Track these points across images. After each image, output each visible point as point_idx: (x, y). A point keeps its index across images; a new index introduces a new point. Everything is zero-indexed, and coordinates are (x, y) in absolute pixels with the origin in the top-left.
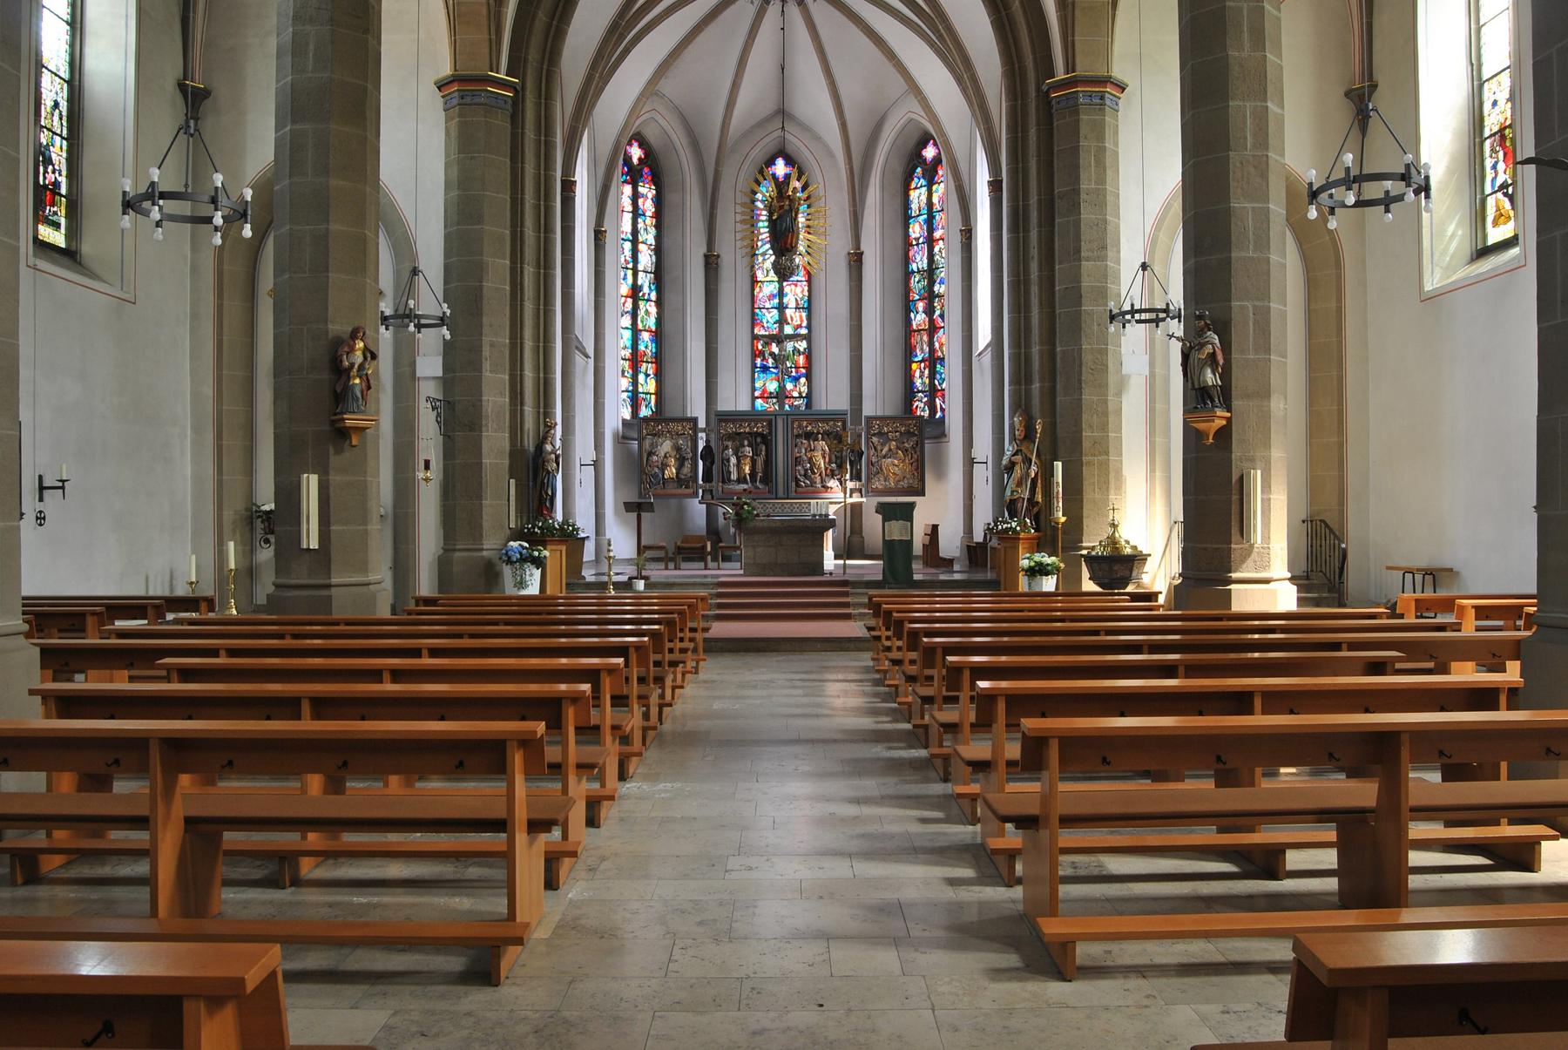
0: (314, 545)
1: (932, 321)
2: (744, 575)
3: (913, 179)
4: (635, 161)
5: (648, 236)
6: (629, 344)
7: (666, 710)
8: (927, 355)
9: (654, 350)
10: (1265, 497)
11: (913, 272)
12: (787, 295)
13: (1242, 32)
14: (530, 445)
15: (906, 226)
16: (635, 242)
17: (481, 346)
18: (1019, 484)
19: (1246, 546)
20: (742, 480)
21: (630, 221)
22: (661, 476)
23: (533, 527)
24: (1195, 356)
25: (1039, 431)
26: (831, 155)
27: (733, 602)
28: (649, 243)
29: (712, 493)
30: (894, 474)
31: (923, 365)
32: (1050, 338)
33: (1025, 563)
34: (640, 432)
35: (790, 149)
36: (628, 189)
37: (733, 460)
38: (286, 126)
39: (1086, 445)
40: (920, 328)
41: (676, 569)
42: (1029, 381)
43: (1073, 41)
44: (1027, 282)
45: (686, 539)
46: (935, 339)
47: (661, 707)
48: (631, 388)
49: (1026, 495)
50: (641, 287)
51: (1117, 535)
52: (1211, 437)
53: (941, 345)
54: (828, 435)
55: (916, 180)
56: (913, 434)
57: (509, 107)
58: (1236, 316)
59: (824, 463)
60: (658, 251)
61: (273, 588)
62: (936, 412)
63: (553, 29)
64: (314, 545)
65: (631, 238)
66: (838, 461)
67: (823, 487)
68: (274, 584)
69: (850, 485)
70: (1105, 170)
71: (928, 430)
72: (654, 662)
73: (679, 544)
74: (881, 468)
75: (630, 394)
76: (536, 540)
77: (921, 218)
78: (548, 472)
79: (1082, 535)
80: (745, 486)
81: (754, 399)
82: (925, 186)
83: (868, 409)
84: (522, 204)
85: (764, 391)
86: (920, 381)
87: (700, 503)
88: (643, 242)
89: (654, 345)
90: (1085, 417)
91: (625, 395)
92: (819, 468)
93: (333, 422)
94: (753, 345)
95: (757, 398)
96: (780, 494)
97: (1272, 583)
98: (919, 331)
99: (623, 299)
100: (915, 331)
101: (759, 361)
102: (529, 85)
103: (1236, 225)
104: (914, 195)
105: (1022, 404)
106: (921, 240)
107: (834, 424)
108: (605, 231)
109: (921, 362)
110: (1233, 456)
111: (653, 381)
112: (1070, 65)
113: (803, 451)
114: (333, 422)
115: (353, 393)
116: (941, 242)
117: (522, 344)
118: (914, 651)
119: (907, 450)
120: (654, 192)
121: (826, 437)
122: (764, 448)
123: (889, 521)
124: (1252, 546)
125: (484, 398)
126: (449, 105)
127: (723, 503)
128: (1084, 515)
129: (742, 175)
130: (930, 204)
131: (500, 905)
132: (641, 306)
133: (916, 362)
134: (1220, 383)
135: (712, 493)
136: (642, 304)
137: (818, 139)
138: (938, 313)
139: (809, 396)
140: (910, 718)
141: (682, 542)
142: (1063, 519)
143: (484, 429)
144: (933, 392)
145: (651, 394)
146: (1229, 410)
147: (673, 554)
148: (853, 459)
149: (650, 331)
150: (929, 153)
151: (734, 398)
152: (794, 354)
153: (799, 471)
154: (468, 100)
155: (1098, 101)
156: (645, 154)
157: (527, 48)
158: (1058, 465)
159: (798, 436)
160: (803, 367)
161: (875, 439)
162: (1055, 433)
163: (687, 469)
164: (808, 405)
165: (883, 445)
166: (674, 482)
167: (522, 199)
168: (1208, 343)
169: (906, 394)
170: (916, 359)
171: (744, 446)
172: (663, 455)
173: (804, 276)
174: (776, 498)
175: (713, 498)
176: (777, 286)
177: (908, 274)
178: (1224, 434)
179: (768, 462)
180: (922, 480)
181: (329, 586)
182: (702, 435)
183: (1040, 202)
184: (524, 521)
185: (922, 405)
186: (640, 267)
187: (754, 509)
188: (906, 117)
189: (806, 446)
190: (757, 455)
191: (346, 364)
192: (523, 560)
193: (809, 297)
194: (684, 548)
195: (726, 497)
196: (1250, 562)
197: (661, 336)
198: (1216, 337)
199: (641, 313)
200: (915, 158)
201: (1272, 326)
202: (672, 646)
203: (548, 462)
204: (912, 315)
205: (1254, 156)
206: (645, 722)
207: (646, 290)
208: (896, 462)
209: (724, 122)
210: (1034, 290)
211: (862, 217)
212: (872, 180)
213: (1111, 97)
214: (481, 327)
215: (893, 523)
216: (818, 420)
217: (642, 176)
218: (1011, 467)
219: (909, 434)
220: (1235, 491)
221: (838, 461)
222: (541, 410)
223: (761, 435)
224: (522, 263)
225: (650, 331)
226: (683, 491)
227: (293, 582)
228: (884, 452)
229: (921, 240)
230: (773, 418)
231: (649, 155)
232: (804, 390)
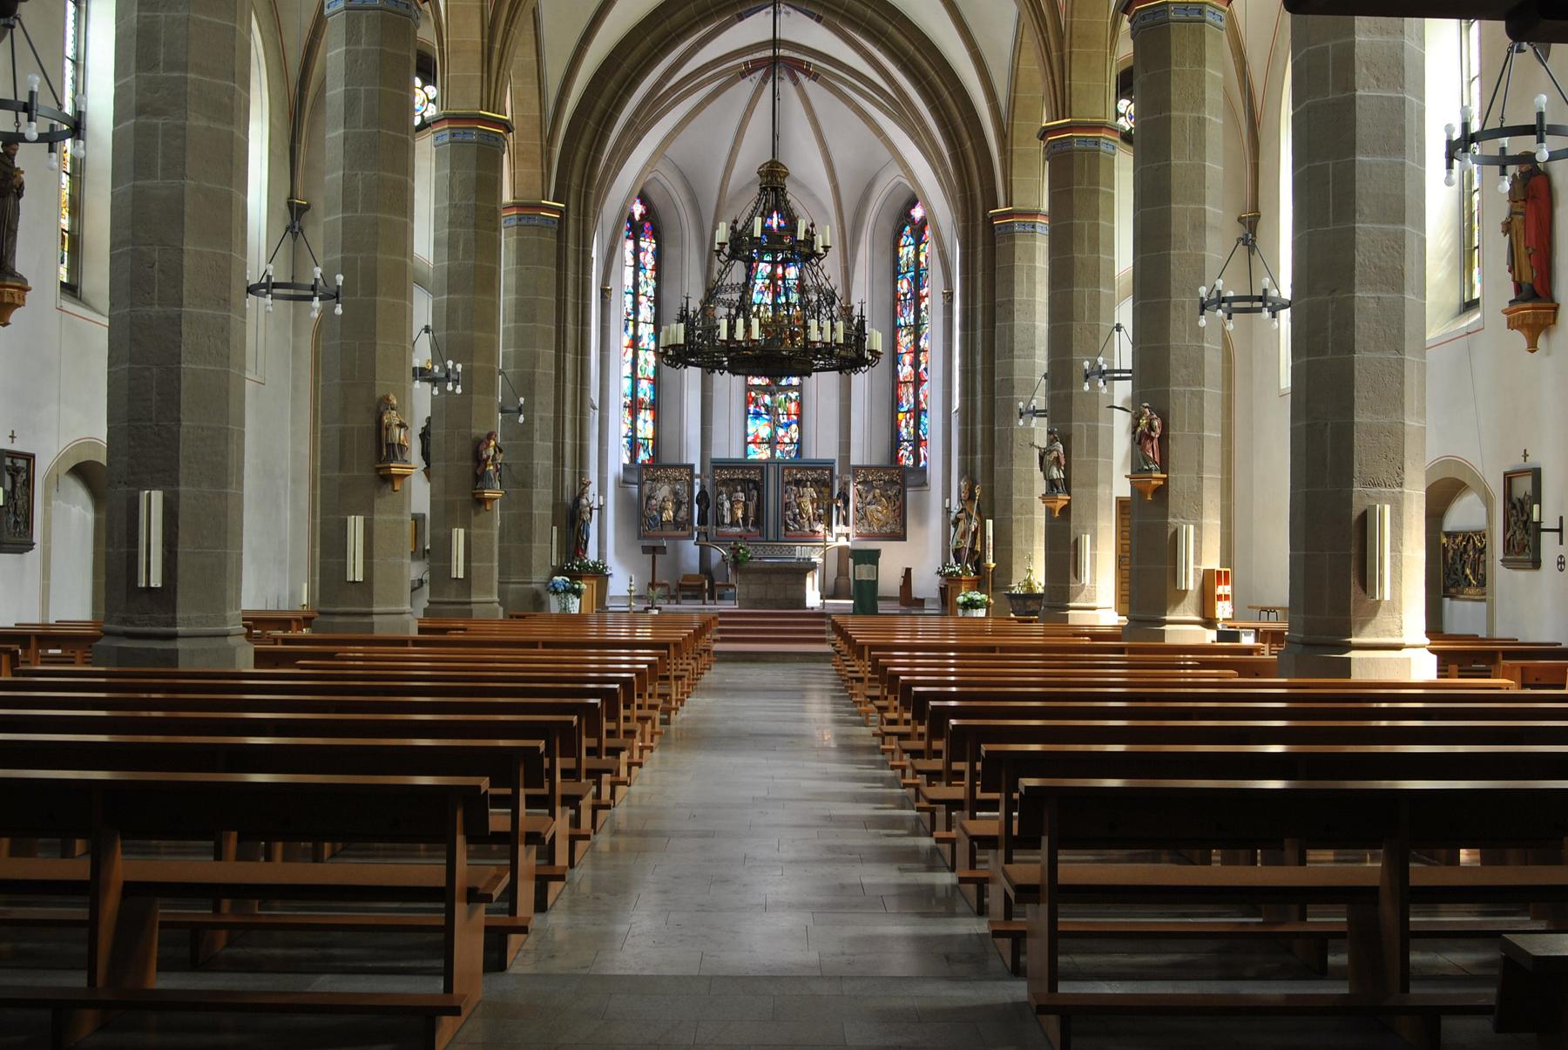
0: (461, 576)
2: (739, 608)
4: (637, 217)
5: (648, 288)
6: (628, 391)
7: (602, 814)
8: (912, 406)
9: (652, 397)
10: (1093, 552)
11: (901, 326)
13: (1083, 240)
14: (568, 498)
16: (636, 294)
17: (533, 420)
18: (963, 536)
19: (1080, 585)
20: (734, 523)
21: (632, 275)
22: (659, 518)
23: (572, 565)
24: (1047, 458)
25: (978, 494)
26: (825, 212)
27: (731, 627)
28: (649, 294)
29: (706, 536)
30: (878, 519)
31: (908, 415)
32: (990, 419)
33: (960, 599)
34: (640, 476)
36: (630, 245)
37: (727, 505)
38: (442, 295)
39: (1016, 506)
40: (906, 380)
41: (677, 603)
42: (974, 452)
43: (1011, 180)
44: (974, 372)
45: (686, 577)
47: (573, 840)
48: (630, 434)
49: (968, 545)
50: (641, 337)
51: (1032, 578)
52: (1057, 512)
53: (926, 397)
54: (816, 483)
55: (905, 238)
57: (556, 226)
58: (1075, 432)
61: (428, 604)
62: (919, 461)
63: (590, 158)
64: (461, 576)
65: (632, 291)
67: (811, 531)
68: (428, 601)
70: (1035, 285)
71: (911, 479)
72: (608, 732)
73: (680, 581)
74: (865, 514)
75: (629, 439)
76: (575, 576)
77: (909, 275)
78: (584, 521)
79: (1012, 578)
80: (738, 530)
81: (746, 444)
83: (856, 459)
84: (565, 304)
85: (757, 437)
86: (905, 430)
87: (695, 544)
88: (643, 295)
89: (652, 393)
90: (1015, 484)
91: (625, 441)
92: (807, 513)
93: (474, 494)
94: (746, 394)
95: (750, 443)
96: (771, 537)
97: (1403, 650)
98: (905, 382)
100: (901, 383)
101: (752, 408)
102: (571, 206)
103: (1076, 371)
104: (903, 252)
105: (967, 472)
107: (822, 473)
108: (611, 290)
109: (907, 412)
110: (1072, 525)
112: (1009, 203)
113: (793, 497)
114: (474, 494)
115: (490, 475)
116: (926, 299)
117: (563, 417)
118: (997, 792)
119: (890, 498)
120: (654, 246)
124: (1084, 585)
125: (535, 462)
126: (439, 142)
127: (717, 545)
128: (1014, 562)
131: (439, 984)
132: (640, 357)
134: (1062, 476)
135: (706, 536)
136: (641, 353)
137: (812, 195)
138: (923, 366)
139: (800, 442)
140: (933, 828)
141: (683, 580)
142: (993, 565)
143: (534, 486)
144: (917, 442)
145: (648, 439)
146: (1069, 495)
147: (676, 590)
150: (917, 213)
151: (727, 447)
152: (786, 402)
154: (524, 222)
155: (1031, 229)
157: (570, 177)
158: (990, 523)
159: (789, 483)
161: (859, 487)
162: (993, 494)
163: (683, 513)
164: (799, 452)
167: (566, 300)
168: (1054, 450)
169: (892, 442)
170: (902, 410)
172: (661, 499)
174: (767, 541)
175: (707, 540)
178: (1066, 510)
179: (760, 508)
180: (904, 526)
181: (470, 603)
182: (697, 481)
183: (984, 307)
184: (564, 559)
185: (907, 454)
186: (641, 318)
187: (748, 552)
188: (895, 180)
191: (485, 456)
192: (567, 591)
194: (686, 586)
195: (721, 540)
196: (1082, 595)
198: (1061, 446)
199: (641, 362)
200: (904, 217)
201: (1099, 438)
202: (629, 714)
203: (584, 513)
204: (899, 367)
205: (1089, 325)
206: (595, 800)
209: (722, 183)
210: (979, 378)
211: (853, 273)
213: (1212, 10)
214: (534, 404)
216: (807, 468)
217: (643, 231)
218: (956, 522)
219: (892, 482)
220: (1072, 548)
222: (577, 470)
223: (754, 482)
224: (564, 352)
226: (680, 533)
227: (446, 600)
228: (868, 499)
230: (765, 465)
231: (650, 212)
232: (795, 436)
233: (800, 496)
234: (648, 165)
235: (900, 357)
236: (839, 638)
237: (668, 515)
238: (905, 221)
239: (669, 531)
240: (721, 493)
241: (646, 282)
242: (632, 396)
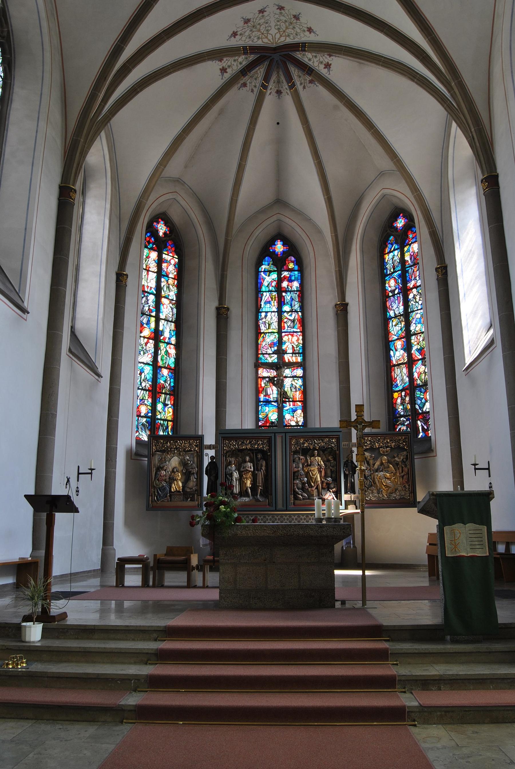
1: (410, 355)
3: (387, 246)
4: (161, 234)
6: (149, 376)
9: (172, 384)
12: (285, 343)
15: (383, 283)
20: (243, 493)
26: (319, 231)
30: (386, 486)
31: (403, 393)
35: (286, 232)
36: (154, 255)
37: (236, 475)
46: (414, 370)
50: (162, 331)
54: (323, 452)
55: (389, 246)
56: (403, 449)
59: (321, 477)
60: (179, 304)
65: (155, 292)
66: (333, 475)
69: (345, 497)
74: (374, 481)
80: (247, 499)
82: (397, 249)
86: (401, 407)
88: (165, 297)
89: (172, 380)
92: (316, 481)
96: (280, 506)
98: (399, 365)
99: (146, 340)
100: (395, 366)
101: (262, 397)
106: (396, 292)
107: (329, 441)
109: (401, 391)
111: (171, 410)
113: (301, 466)
116: (414, 290)
119: (397, 464)
121: (321, 453)
122: (264, 463)
123: (450, 524)
129: (248, 248)
130: (403, 261)
132: (162, 348)
133: (397, 391)
136: (162, 346)
137: (308, 220)
145: (168, 421)
148: (347, 473)
149: (168, 368)
153: (297, 484)
156: (170, 231)
159: (296, 452)
160: (299, 401)
161: (367, 454)
163: (192, 483)
165: (375, 459)
166: (181, 495)
169: (389, 418)
171: (245, 462)
172: (171, 470)
173: (299, 328)
174: (276, 510)
176: (277, 336)
177: (386, 321)
186: (162, 316)
189: (303, 461)
190: (258, 470)
193: (304, 344)
197: (179, 372)
199: (162, 352)
204: (392, 353)
207: (167, 334)
208: (388, 475)
209: (232, 199)
212: (354, 247)
215: (458, 527)
216: (314, 437)
219: (399, 449)
221: (333, 475)
223: (261, 451)
225: (168, 368)
226: (189, 503)
228: (376, 466)
229: (396, 292)
230: (273, 435)
233: (308, 465)
234: (161, 165)
235: (391, 344)
236: (150, 408)
237: (178, 485)
238: (389, 231)
239: (178, 502)
240: (230, 464)
241: (168, 287)
242: (152, 382)
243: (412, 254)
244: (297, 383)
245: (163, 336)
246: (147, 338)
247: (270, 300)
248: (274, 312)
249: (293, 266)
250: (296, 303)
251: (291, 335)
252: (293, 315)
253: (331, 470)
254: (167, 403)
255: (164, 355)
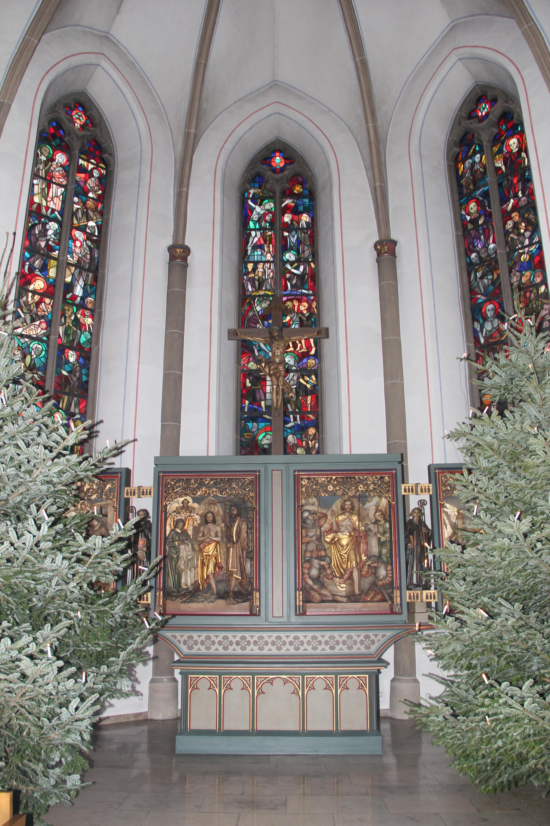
99: (37, 298)
243: (507, 156)
244: (307, 382)
245: (70, 294)
246: (38, 294)
247: (262, 242)
248: (268, 262)
249: (301, 190)
250: (306, 248)
251: (297, 299)
252: (302, 268)
253: (379, 539)
254: (72, 409)
255: (71, 325)
